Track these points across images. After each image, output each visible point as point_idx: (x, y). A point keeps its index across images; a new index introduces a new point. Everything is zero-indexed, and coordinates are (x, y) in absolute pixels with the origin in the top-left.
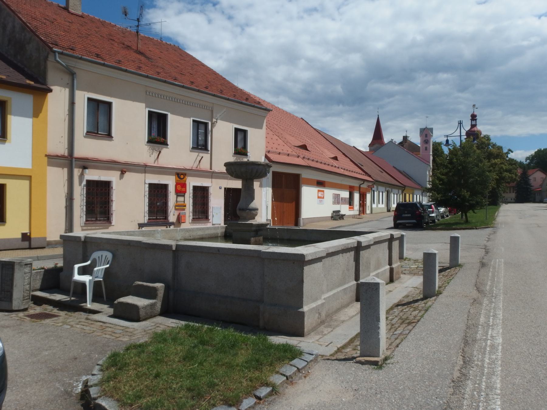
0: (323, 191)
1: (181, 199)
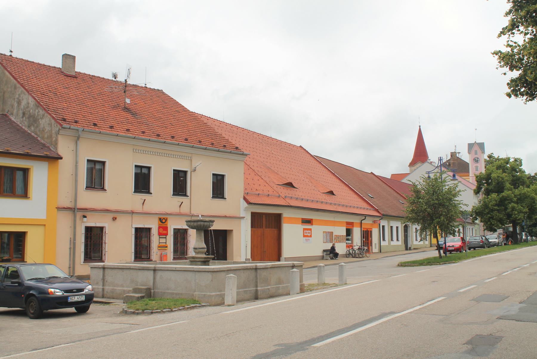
0: (310, 230)
1: (163, 240)
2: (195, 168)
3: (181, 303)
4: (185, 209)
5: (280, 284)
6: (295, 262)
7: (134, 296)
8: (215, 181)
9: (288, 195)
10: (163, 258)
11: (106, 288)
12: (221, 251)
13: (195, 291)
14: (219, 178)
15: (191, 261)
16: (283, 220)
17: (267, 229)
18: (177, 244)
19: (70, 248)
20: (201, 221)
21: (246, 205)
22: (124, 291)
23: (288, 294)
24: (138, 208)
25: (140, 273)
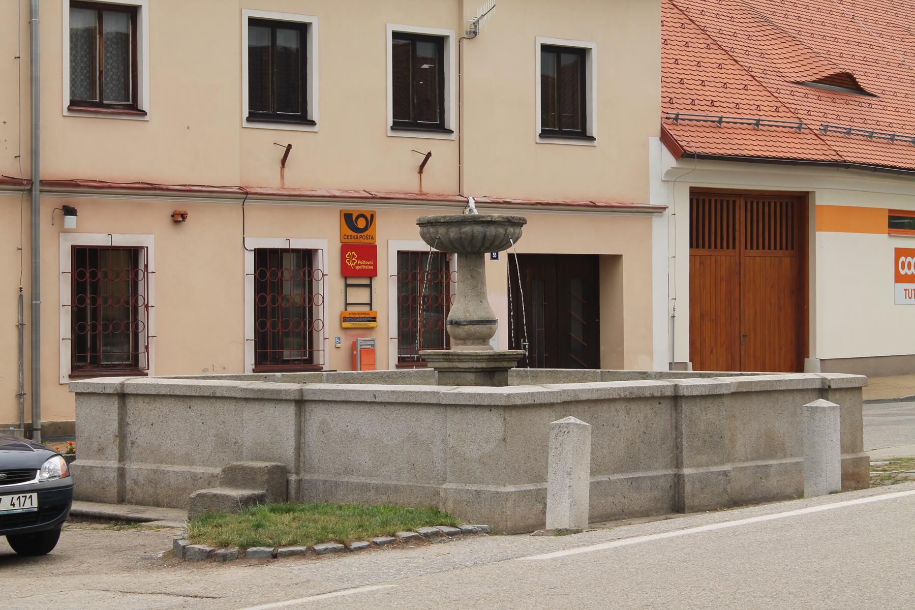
1: (359, 296)
2: (475, 24)
3: (385, 523)
4: (439, 180)
5: (772, 457)
6: (829, 376)
7: (227, 497)
8: (553, 73)
9: (834, 122)
10: (360, 358)
11: (133, 466)
12: (577, 335)
13: (444, 481)
14: (567, 60)
15: (441, 371)
16: (814, 219)
17: (755, 252)
18: (414, 309)
19: (20, 326)
20: (475, 221)
21: (669, 161)
22: (195, 477)
23: (800, 495)
24: (266, 177)
25: (249, 412)
